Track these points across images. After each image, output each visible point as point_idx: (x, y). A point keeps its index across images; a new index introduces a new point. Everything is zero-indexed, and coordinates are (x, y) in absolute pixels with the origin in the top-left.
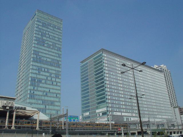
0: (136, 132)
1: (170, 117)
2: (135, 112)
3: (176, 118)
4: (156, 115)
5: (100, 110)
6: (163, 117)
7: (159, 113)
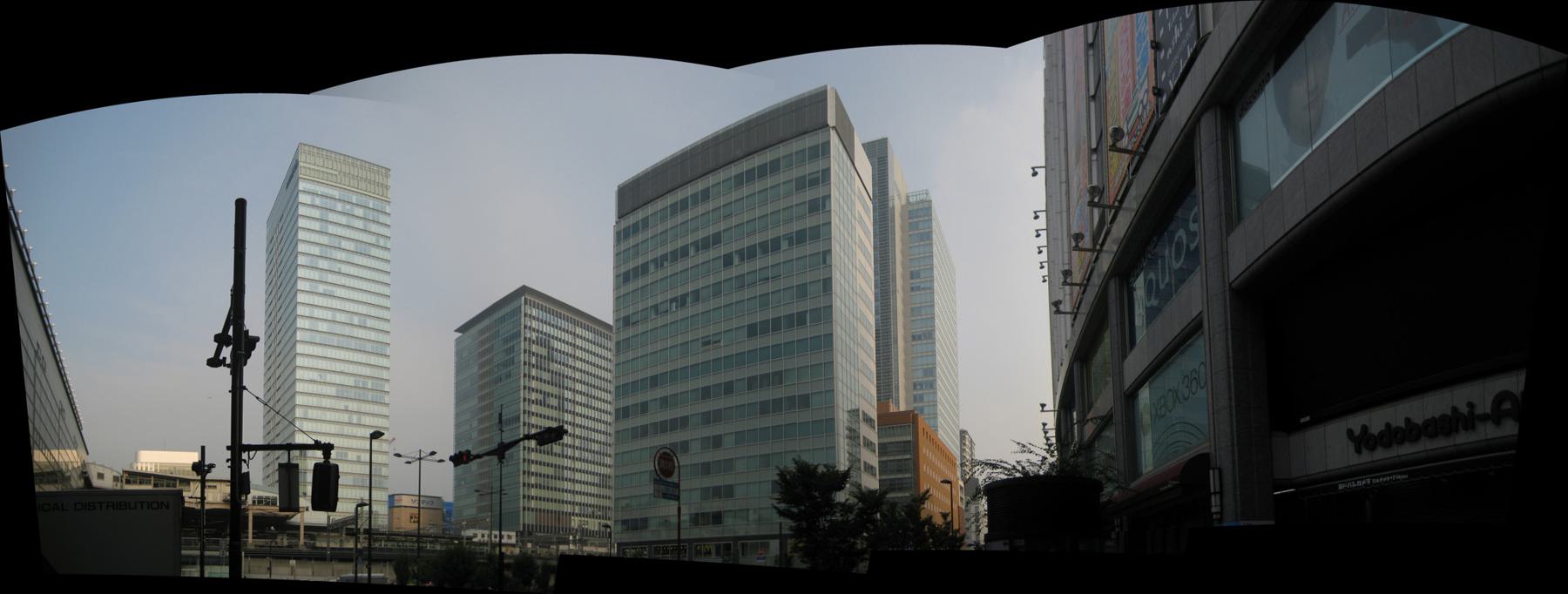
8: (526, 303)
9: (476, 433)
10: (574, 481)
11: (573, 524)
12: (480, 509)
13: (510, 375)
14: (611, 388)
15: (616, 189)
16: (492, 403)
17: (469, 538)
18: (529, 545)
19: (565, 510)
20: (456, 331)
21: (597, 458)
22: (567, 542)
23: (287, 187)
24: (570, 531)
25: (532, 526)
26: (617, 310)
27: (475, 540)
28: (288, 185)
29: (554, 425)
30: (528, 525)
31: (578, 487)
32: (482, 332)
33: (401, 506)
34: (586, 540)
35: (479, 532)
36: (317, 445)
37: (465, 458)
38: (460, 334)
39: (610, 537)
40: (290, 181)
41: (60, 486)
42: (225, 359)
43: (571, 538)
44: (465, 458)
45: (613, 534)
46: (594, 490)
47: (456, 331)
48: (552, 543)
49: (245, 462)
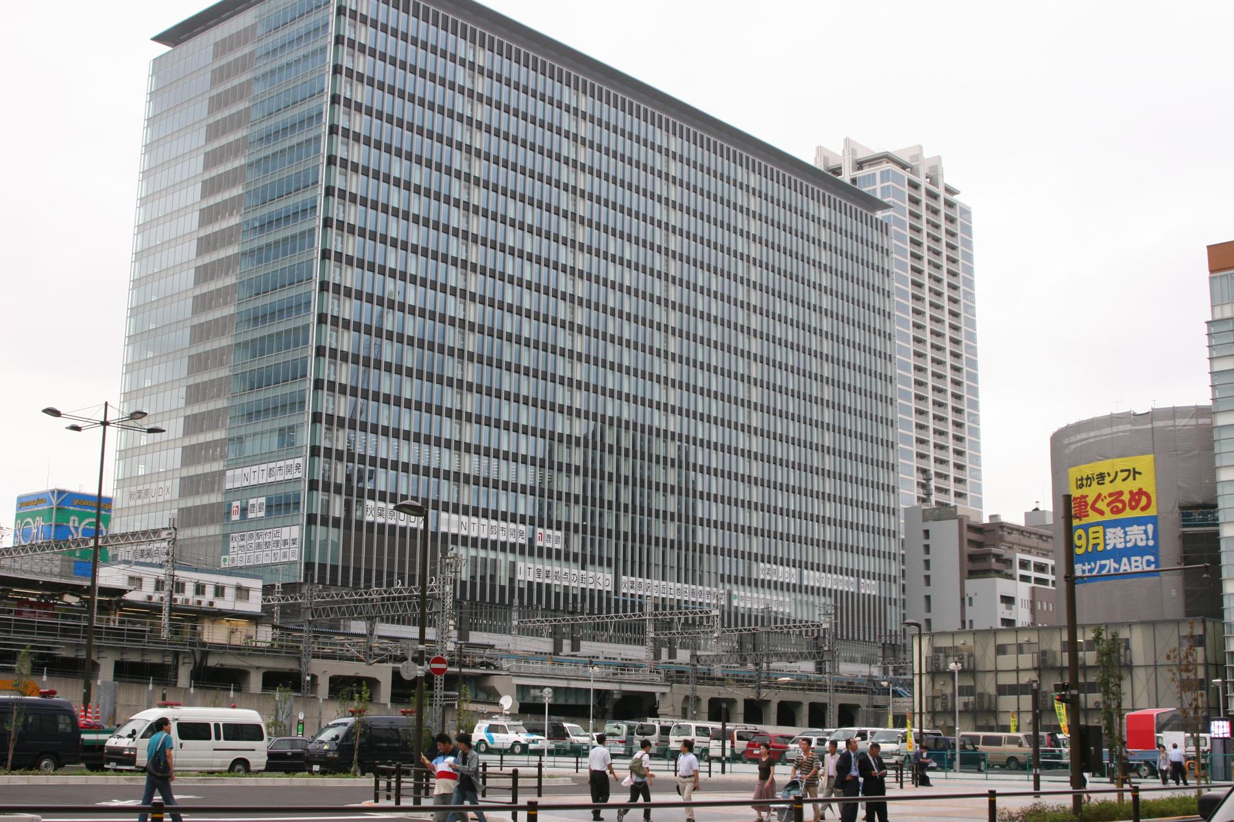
0: (382, 674)
1: (870, 588)
2: (560, 512)
3: (928, 598)
4: (751, 557)
5: (258, 475)
6: (813, 578)
7: (781, 549)
30: (323, 567)
32: (222, 48)
38: (164, 49)
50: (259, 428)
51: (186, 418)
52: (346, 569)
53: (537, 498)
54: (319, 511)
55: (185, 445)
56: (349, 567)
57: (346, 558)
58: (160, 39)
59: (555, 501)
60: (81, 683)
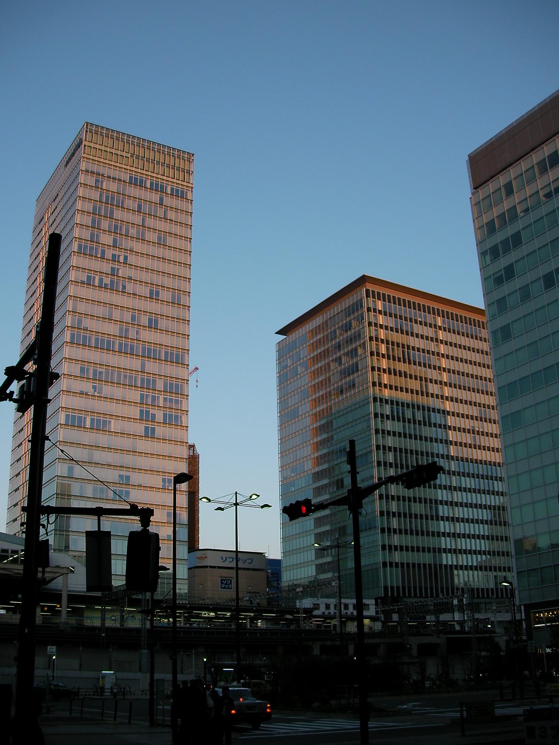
8: (368, 296)
9: (310, 462)
10: (454, 520)
11: (456, 581)
12: (321, 568)
13: (354, 385)
14: (492, 387)
15: (467, 158)
16: (331, 422)
17: (308, 611)
18: (395, 617)
19: (445, 563)
20: (276, 333)
21: (483, 484)
22: (450, 609)
23: (66, 166)
24: (452, 590)
25: (398, 588)
26: (486, 294)
27: (316, 613)
28: (68, 163)
29: (424, 461)
30: (392, 588)
31: (460, 528)
32: (314, 332)
33: (206, 567)
34: (478, 604)
35: (322, 602)
36: (134, 510)
37: (304, 509)
38: (282, 337)
39: (513, 596)
40: (70, 159)
41: (465, 716)
42: (12, 393)
43: (455, 602)
44: (304, 509)
45: (517, 592)
46: (484, 530)
47: (276, 333)
48: (428, 612)
49: (44, 526)
50: (339, 446)
51: (316, 565)
52: (404, 588)
53: (492, 511)
54: (374, 350)
55: (316, 564)
56: (407, 567)
57: (403, 582)
58: (280, 332)
59: (501, 511)
60: (96, 518)
